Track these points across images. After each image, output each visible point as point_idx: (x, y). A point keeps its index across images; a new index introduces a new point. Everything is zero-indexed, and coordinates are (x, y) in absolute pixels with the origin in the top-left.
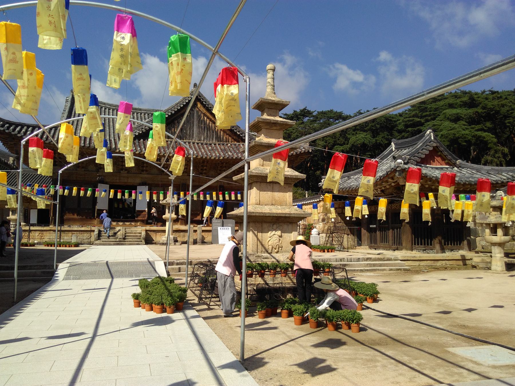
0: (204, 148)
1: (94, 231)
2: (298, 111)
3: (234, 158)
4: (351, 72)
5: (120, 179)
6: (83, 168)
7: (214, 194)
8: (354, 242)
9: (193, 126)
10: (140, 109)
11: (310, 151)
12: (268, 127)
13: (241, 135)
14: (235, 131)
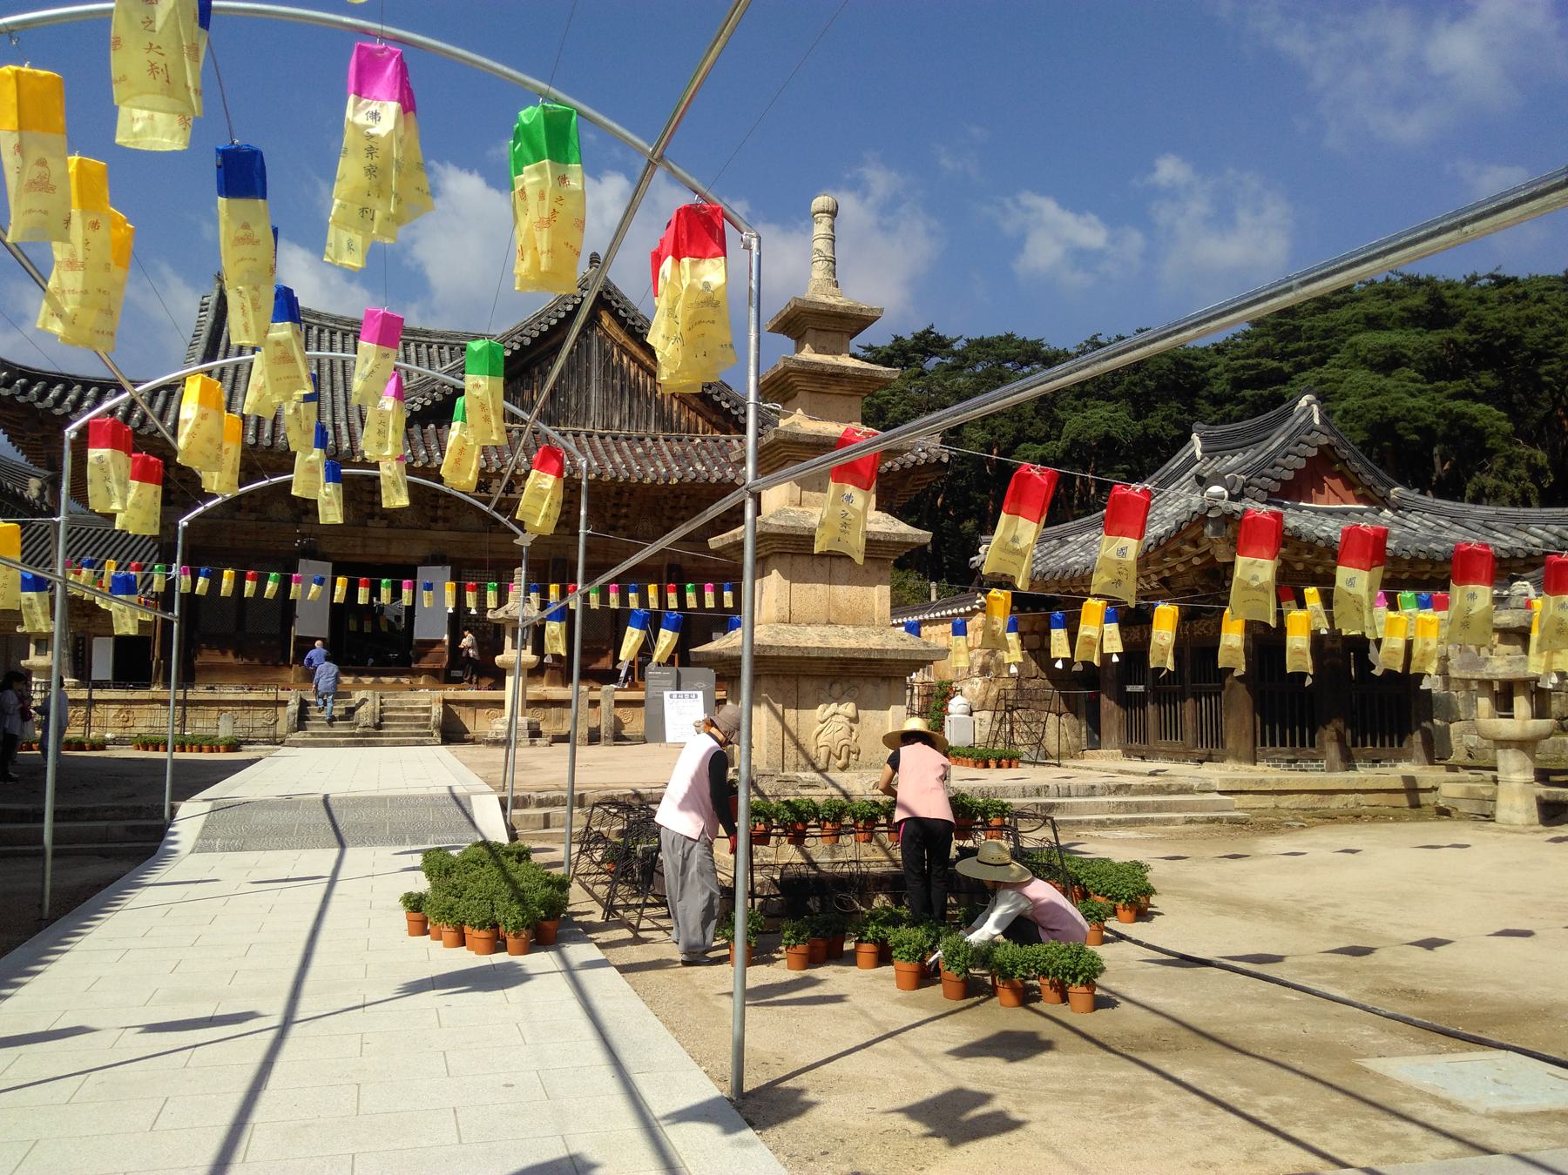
0: (620, 451)
1: (285, 703)
2: (908, 337)
3: (714, 480)
4: (1068, 219)
5: (365, 546)
6: (252, 510)
7: (652, 590)
8: (1079, 736)
9: (588, 383)
10: (427, 333)
11: (945, 460)
12: (816, 387)
13: (735, 412)
14: (716, 398)
